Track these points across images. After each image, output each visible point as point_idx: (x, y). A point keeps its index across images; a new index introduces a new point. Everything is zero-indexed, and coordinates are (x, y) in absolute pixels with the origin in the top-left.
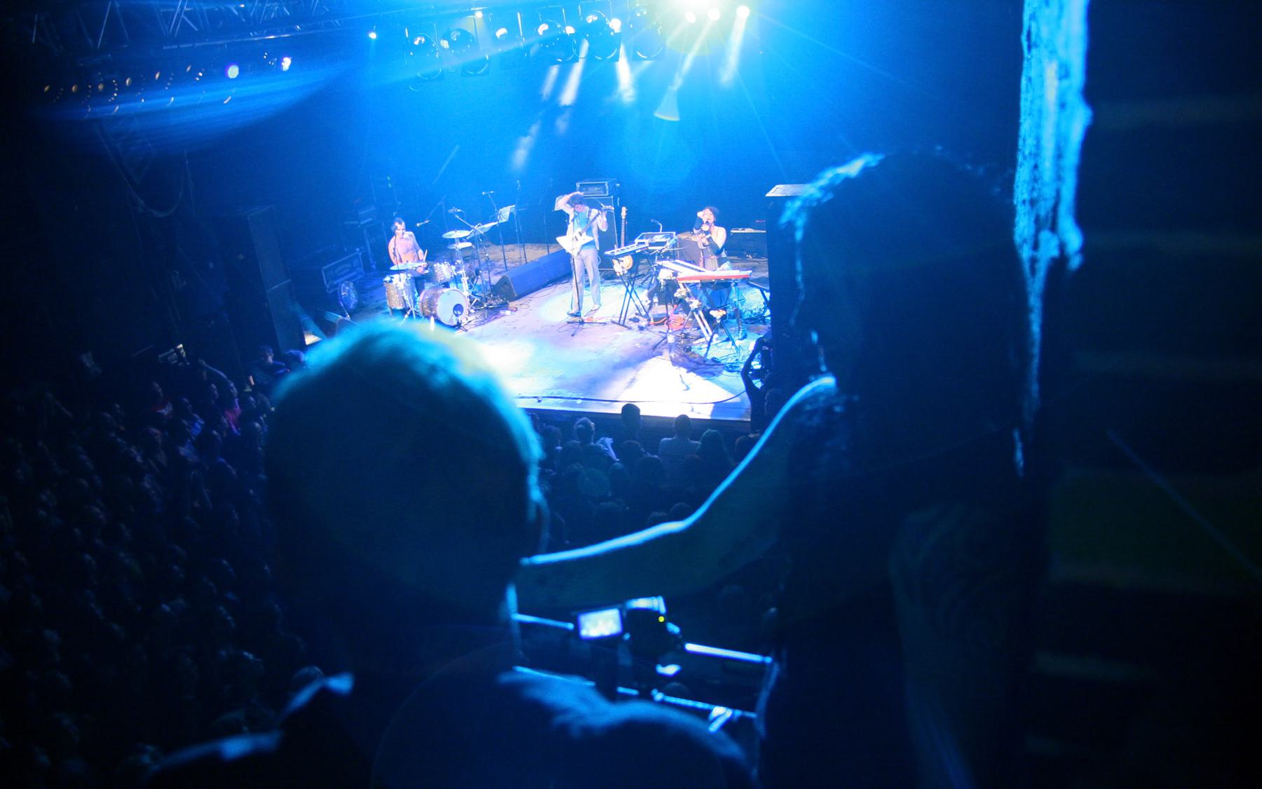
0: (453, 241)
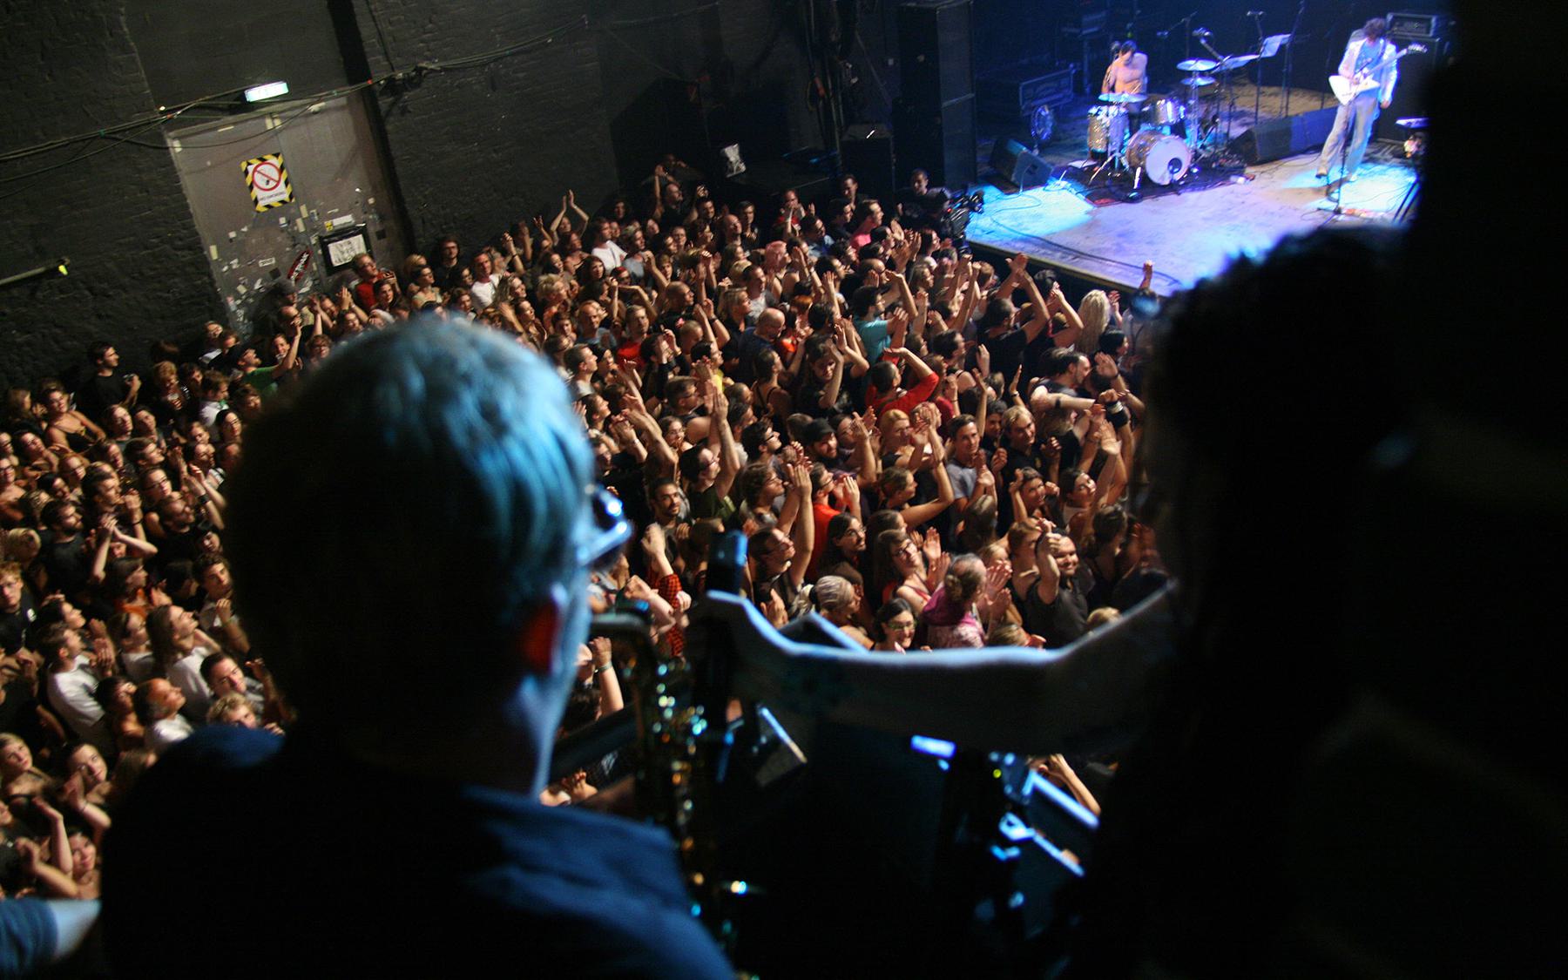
0: (1190, 74)
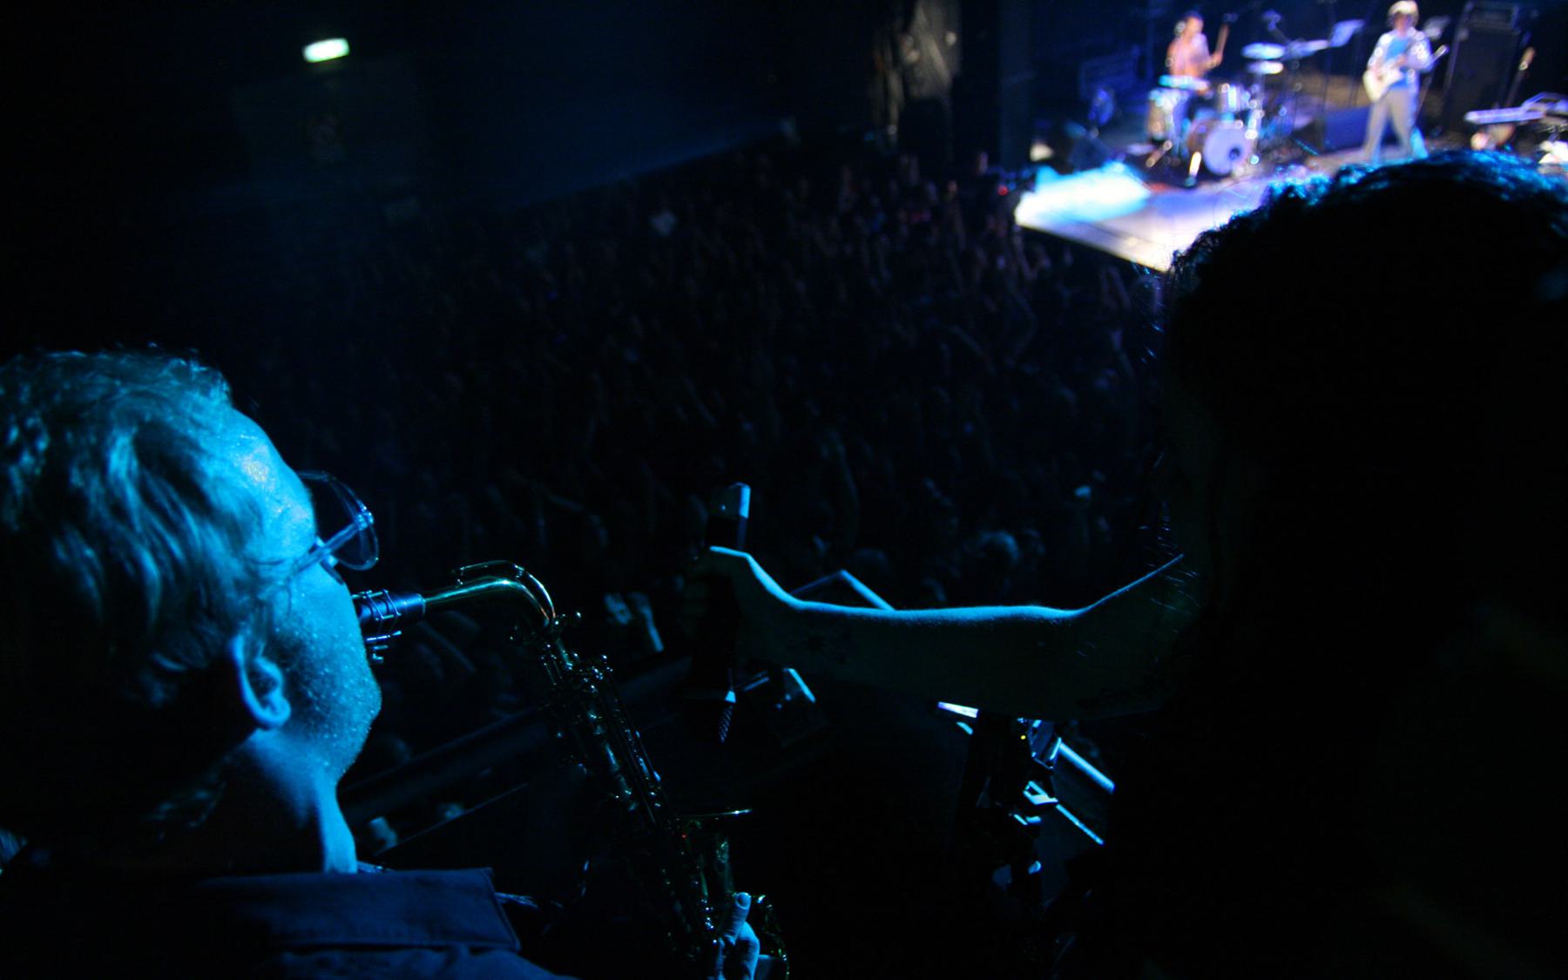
0: (1254, 60)
